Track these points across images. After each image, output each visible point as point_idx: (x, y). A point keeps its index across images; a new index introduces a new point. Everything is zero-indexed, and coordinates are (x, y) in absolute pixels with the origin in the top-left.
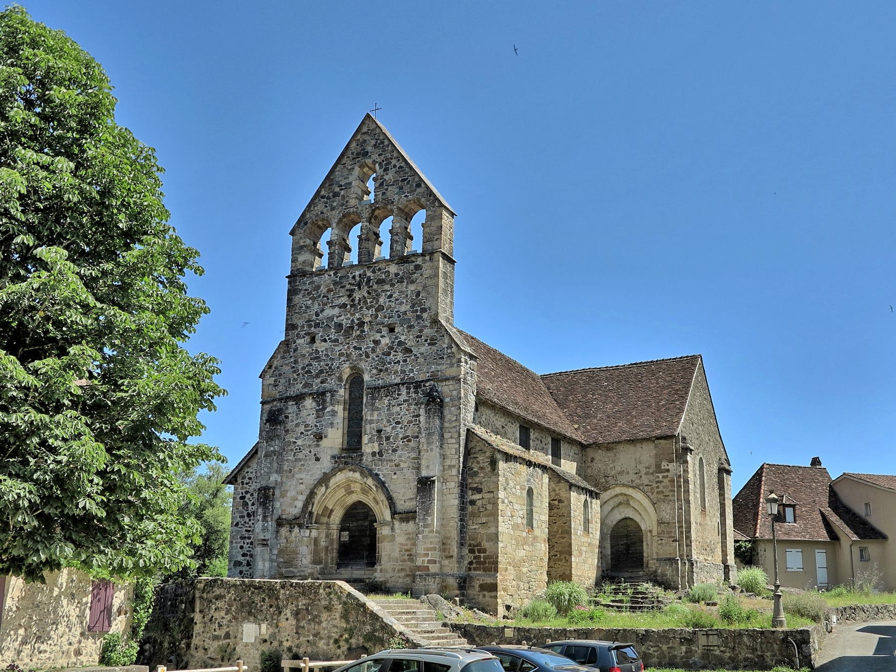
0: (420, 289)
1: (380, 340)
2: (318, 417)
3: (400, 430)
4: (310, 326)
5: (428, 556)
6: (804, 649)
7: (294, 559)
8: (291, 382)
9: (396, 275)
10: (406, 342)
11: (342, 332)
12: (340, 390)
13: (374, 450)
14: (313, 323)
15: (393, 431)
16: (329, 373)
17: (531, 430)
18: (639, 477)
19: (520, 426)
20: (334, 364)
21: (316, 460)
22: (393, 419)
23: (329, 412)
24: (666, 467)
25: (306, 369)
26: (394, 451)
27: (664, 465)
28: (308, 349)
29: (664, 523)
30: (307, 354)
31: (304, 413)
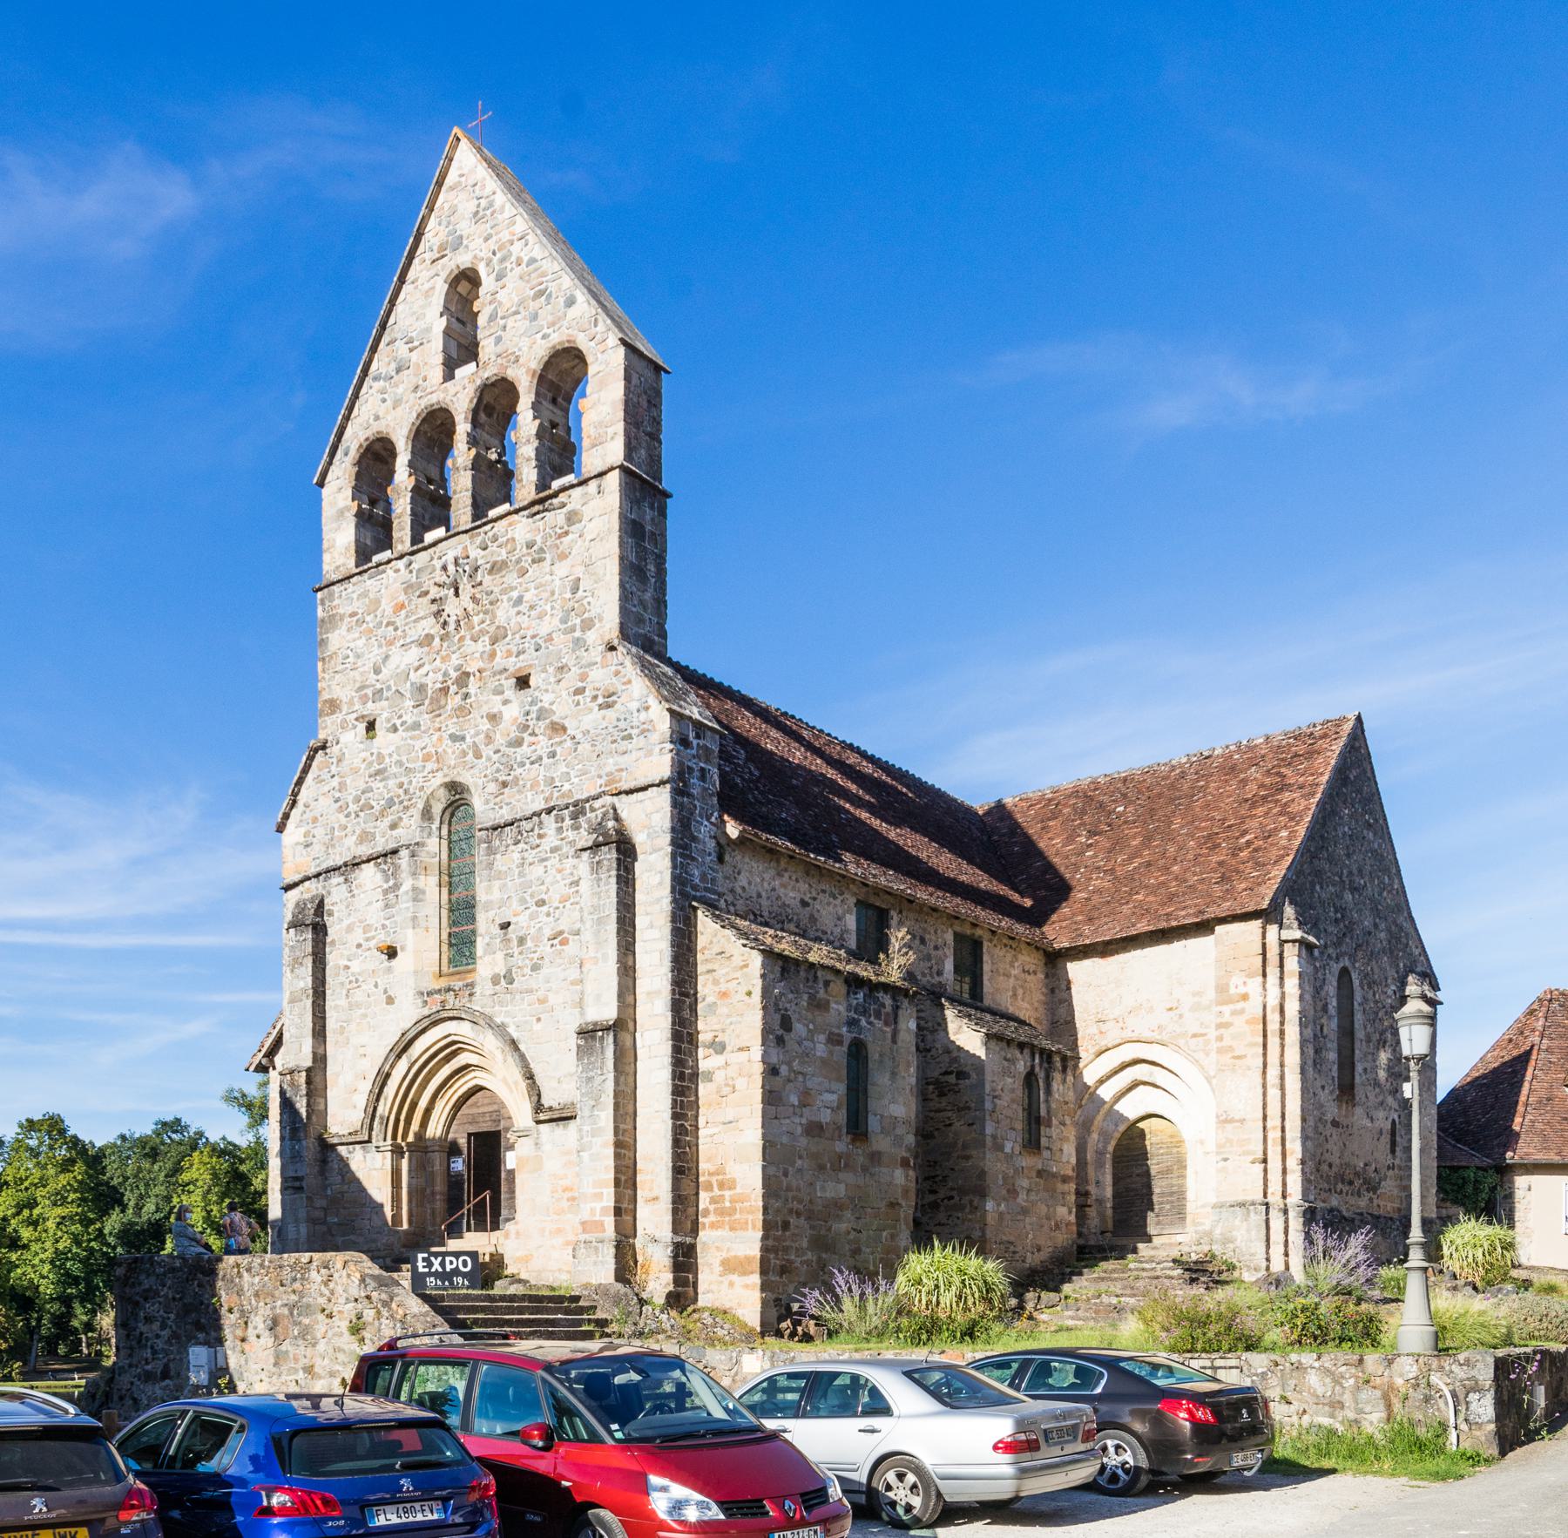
0: (579, 571)
1: (501, 712)
2: (387, 906)
3: (545, 919)
4: (364, 701)
5: (602, 1199)
6: (1473, 1407)
7: (357, 1216)
8: (336, 833)
9: (530, 545)
10: (554, 707)
11: (427, 702)
12: (429, 841)
13: (497, 971)
14: (369, 692)
15: (532, 923)
16: (405, 803)
17: (893, 913)
18: (1175, 1018)
19: (859, 903)
20: (414, 780)
21: (388, 1003)
22: (532, 896)
23: (407, 892)
24: (1242, 990)
25: (362, 801)
26: (535, 968)
28: (364, 755)
29: (1232, 1121)
30: (363, 766)
31: (361, 900)
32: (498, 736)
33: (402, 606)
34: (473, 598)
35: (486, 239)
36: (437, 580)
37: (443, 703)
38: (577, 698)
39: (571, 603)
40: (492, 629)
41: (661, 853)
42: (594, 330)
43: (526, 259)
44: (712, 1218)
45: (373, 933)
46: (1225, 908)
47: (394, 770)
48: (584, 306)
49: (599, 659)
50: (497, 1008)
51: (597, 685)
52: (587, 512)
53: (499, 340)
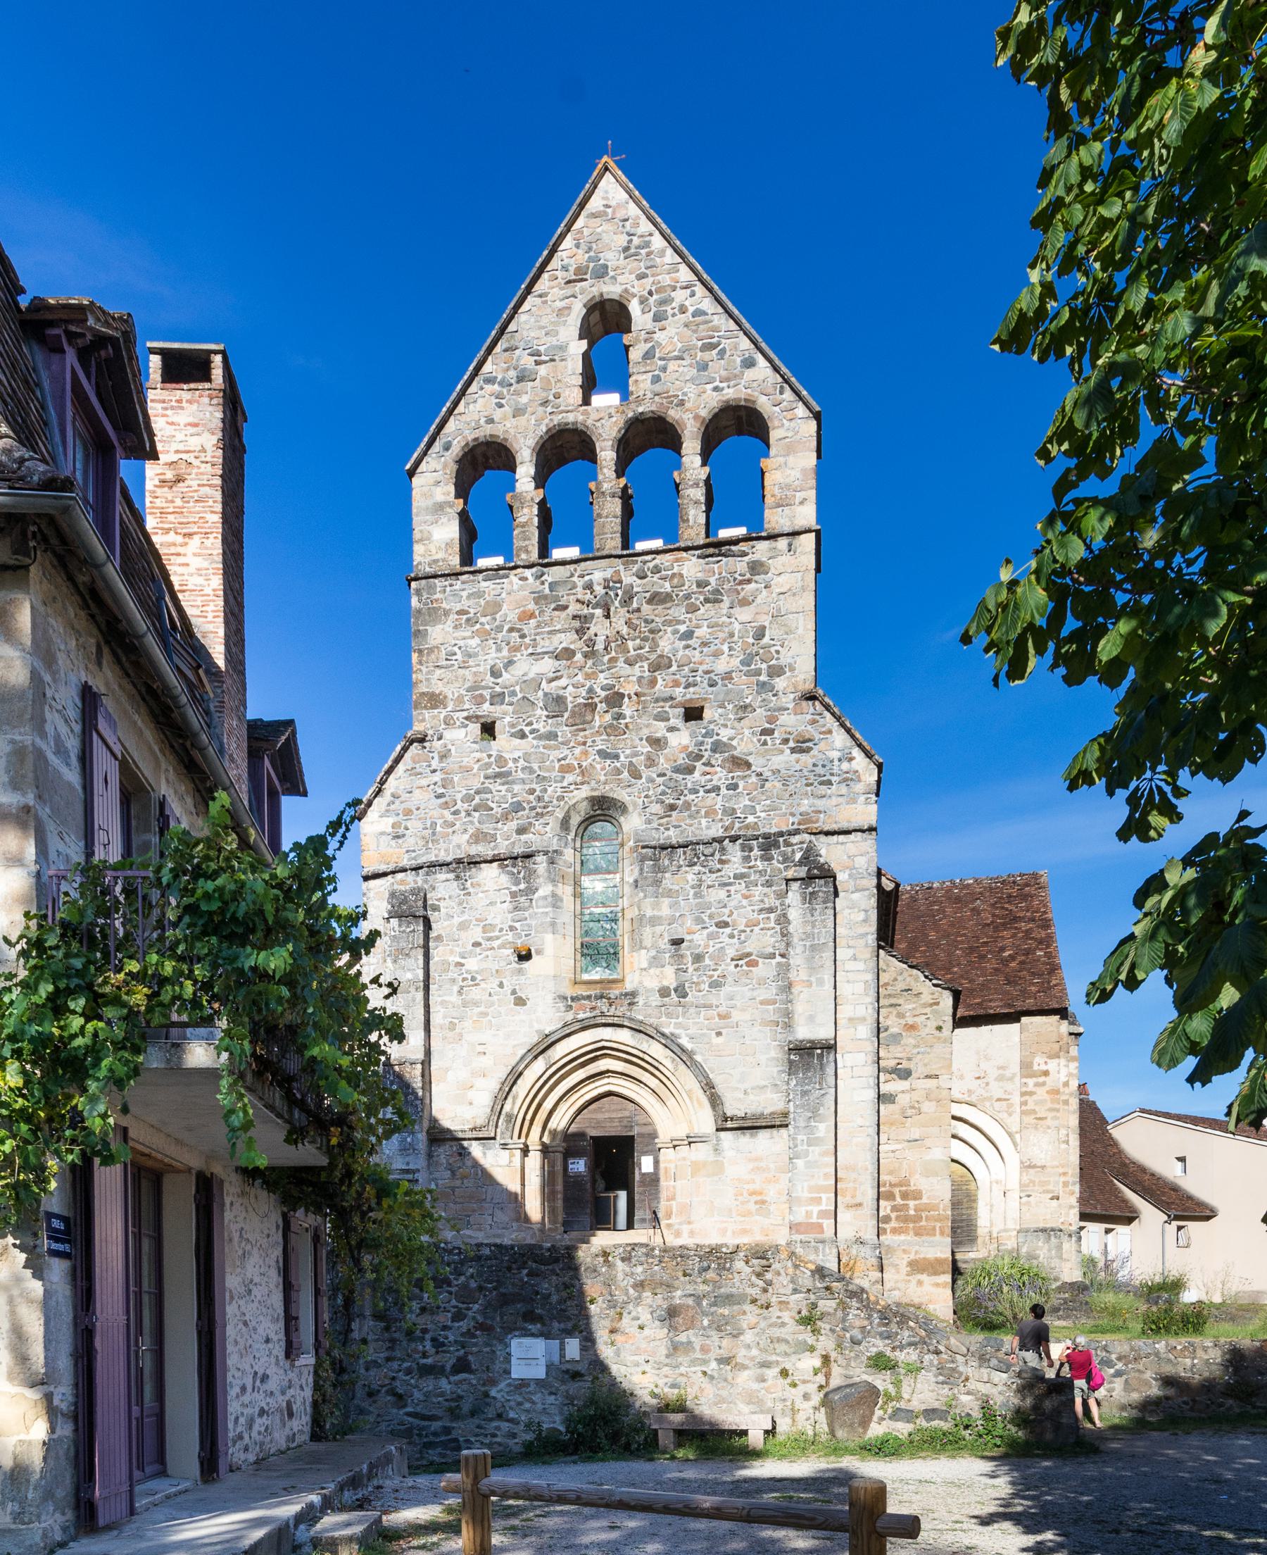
0: (765, 620)
4: (479, 701)
8: (438, 828)
10: (734, 743)
11: (566, 715)
13: (666, 983)
14: (487, 694)
15: (711, 943)
16: (539, 810)
20: (550, 790)
21: (516, 1004)
22: (711, 917)
23: (545, 898)
24: (1044, 1068)
25: (477, 800)
26: (715, 985)
27: (1039, 1063)
28: (478, 755)
29: (1035, 1167)
30: (476, 767)
32: (662, 760)
33: (532, 616)
34: (628, 623)
35: (641, 277)
36: (580, 597)
37: (589, 718)
38: (763, 738)
39: (755, 648)
40: (653, 657)
41: (867, 893)
42: (779, 397)
43: (691, 309)
44: (893, 1224)
45: (497, 933)
46: (1030, 1003)
47: (521, 775)
48: (151, 395)
49: (791, 706)
50: (664, 1019)
51: (789, 729)
52: (776, 565)
53: (656, 380)
